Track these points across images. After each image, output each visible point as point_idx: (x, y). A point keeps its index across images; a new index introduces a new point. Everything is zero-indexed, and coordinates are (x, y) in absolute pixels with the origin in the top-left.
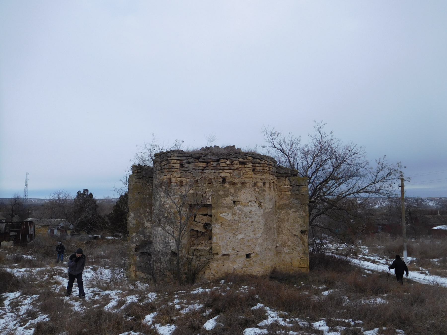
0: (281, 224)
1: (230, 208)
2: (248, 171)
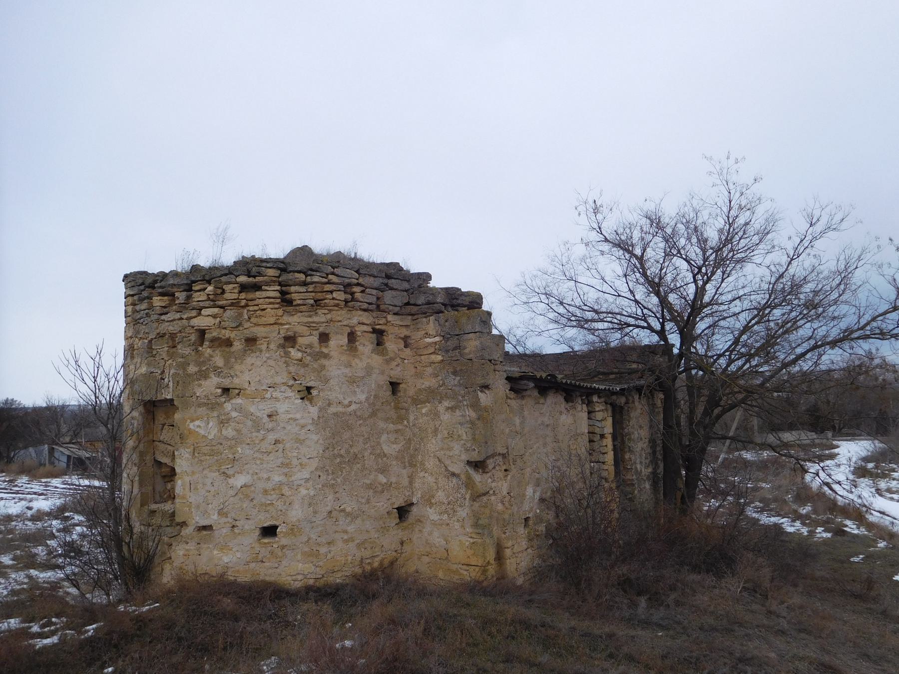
0: (420, 444)
1: (212, 406)
2: (265, 307)
